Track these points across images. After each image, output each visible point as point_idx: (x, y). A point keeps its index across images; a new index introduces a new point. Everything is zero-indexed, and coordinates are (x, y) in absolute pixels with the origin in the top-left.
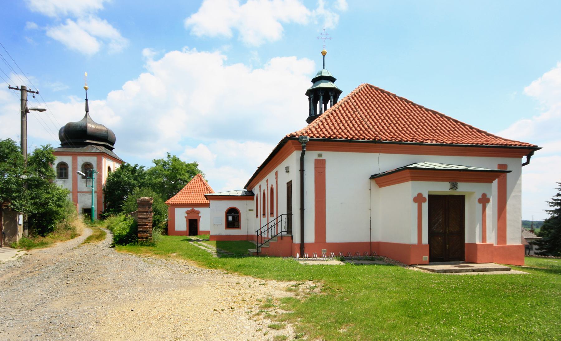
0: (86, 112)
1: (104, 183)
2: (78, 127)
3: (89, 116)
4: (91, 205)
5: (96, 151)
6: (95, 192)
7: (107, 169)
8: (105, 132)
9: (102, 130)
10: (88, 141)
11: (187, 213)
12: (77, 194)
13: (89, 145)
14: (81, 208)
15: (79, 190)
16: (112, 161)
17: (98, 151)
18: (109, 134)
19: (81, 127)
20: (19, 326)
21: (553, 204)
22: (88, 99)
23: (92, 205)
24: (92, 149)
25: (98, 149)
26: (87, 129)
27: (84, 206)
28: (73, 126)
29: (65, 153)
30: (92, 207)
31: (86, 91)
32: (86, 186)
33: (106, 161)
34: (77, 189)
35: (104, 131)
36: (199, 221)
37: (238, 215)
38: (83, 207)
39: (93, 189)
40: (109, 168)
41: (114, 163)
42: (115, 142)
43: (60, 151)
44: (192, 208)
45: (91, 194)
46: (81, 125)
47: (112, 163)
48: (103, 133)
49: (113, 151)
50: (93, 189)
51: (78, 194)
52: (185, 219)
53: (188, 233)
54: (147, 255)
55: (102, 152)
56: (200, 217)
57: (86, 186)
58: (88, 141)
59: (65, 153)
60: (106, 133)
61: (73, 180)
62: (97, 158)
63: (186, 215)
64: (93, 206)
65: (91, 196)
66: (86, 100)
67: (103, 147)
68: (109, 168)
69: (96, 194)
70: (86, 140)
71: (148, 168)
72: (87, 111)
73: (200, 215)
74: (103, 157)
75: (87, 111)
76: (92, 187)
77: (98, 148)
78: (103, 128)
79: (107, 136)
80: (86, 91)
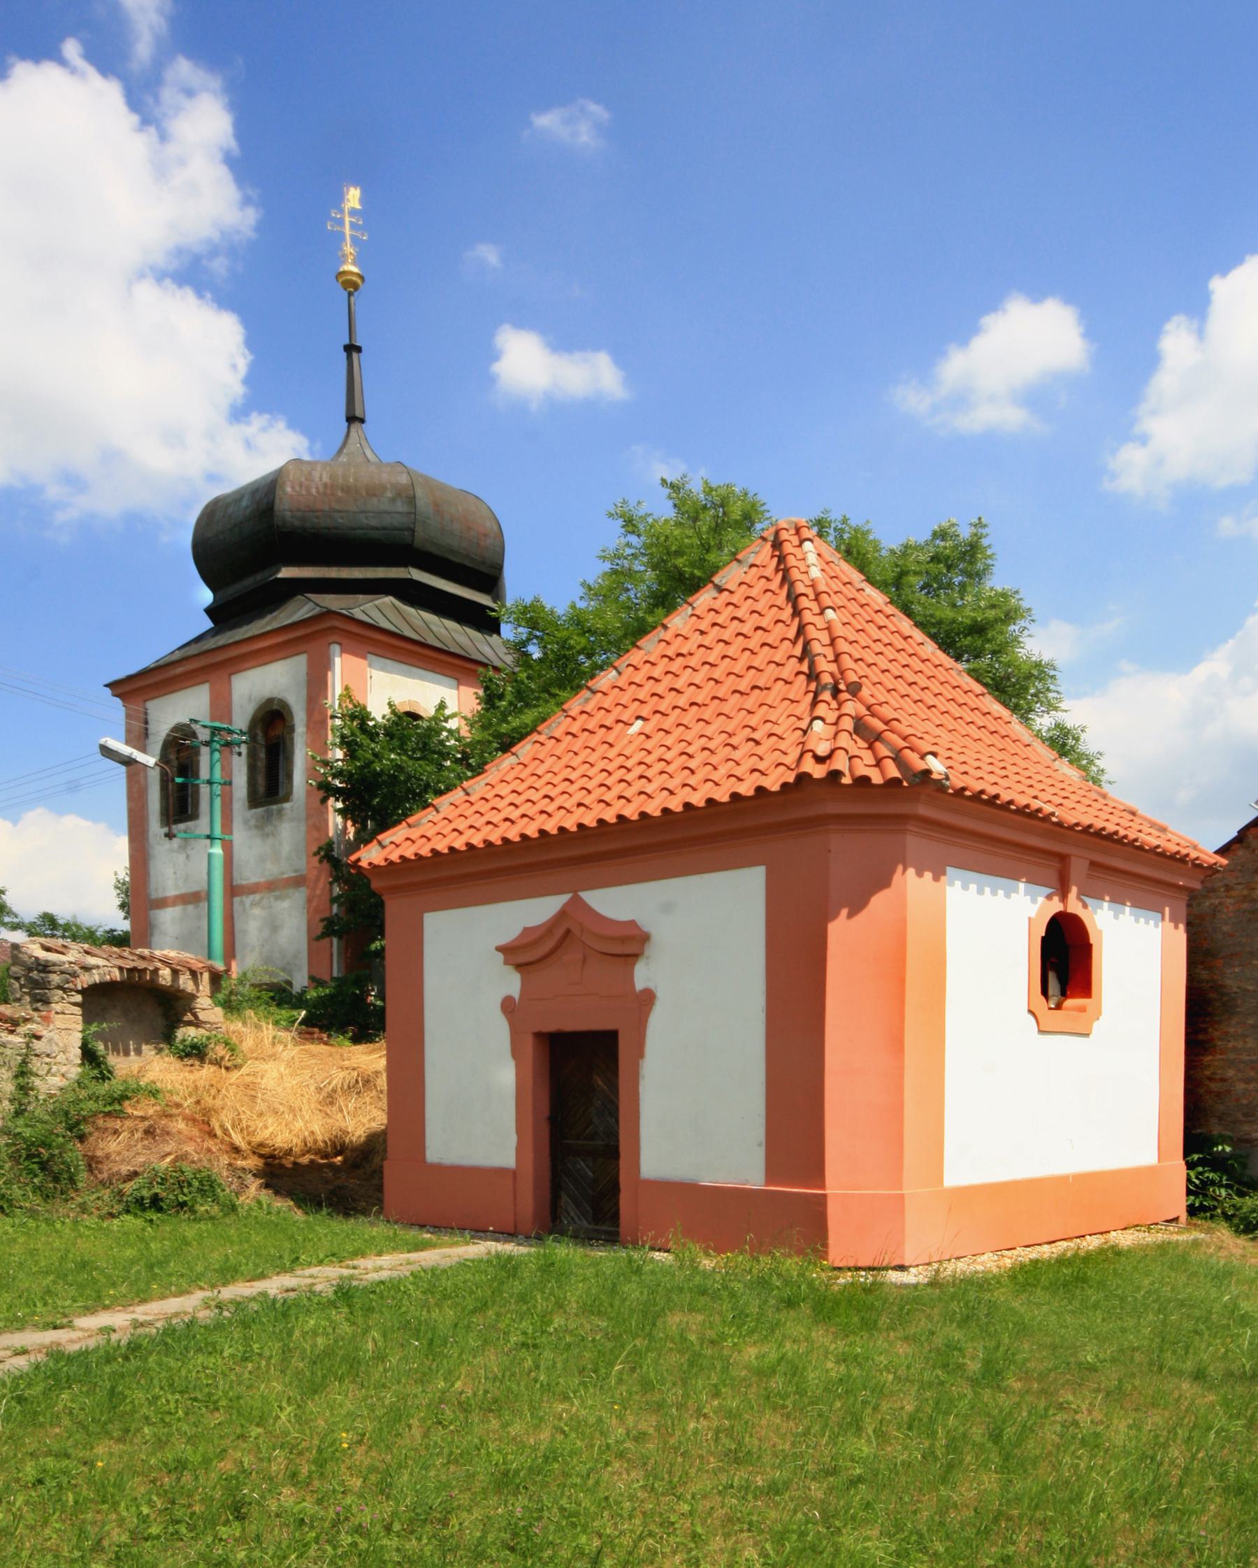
10: (286, 573)
11: (519, 967)
13: (299, 597)
16: (454, 682)
26: (277, 501)
36: (640, 1053)
37: (367, 972)
42: (499, 568)
44: (564, 899)
47: (455, 692)
52: (500, 1030)
53: (527, 1202)
54: (605, 1228)
56: (648, 998)
58: (286, 573)
59: (179, 670)
60: (400, 507)
63: (512, 984)
67: (389, 599)
70: (278, 571)
73: (643, 975)
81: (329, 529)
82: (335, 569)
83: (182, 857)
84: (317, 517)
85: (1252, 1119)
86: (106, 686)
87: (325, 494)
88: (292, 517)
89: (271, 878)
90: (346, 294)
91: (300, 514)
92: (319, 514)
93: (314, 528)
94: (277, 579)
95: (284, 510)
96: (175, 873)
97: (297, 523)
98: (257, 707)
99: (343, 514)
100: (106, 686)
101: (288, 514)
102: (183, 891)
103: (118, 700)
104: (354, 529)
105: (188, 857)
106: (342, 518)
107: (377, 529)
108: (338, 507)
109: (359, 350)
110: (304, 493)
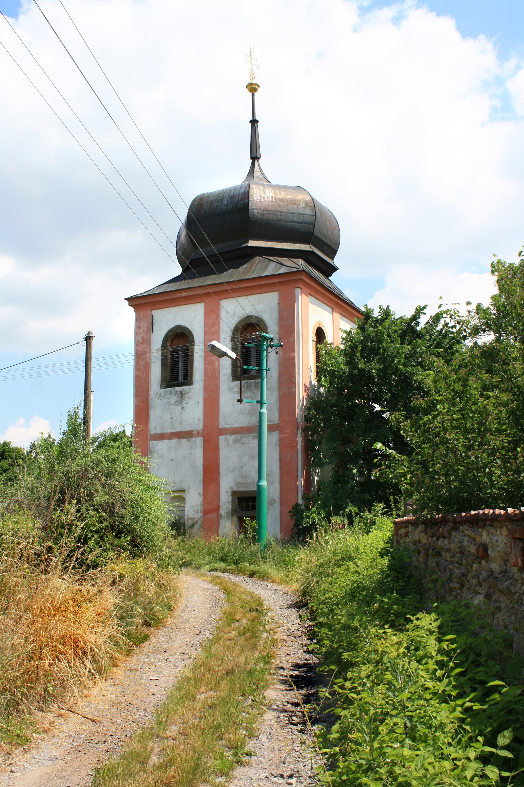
0: (251, 161)
1: (301, 397)
2: (225, 202)
3: (261, 171)
4: (256, 478)
5: (279, 269)
6: (271, 428)
7: (312, 336)
8: (305, 208)
9: (295, 202)
10: (252, 243)
12: (218, 440)
14: (230, 494)
15: (223, 424)
16: (331, 310)
17: (283, 270)
18: (318, 213)
19: (232, 197)
20: (486, 493)
21: (465, 580)
22: (257, 118)
23: (260, 478)
24: (265, 268)
25: (283, 264)
26: (251, 199)
27: (237, 484)
28: (212, 202)
29: (184, 294)
30: (259, 487)
31: (253, 95)
32: (240, 401)
33: (311, 305)
34: (218, 420)
35: (302, 205)
38: (235, 489)
39: (264, 410)
40: (320, 334)
41: (337, 315)
43: (173, 289)
45: (256, 434)
46: (232, 194)
48: (301, 209)
49: (334, 278)
50: (264, 410)
51: (222, 438)
55: (295, 270)
57: (240, 401)
58: (252, 243)
59: (184, 294)
60: (308, 211)
61: (206, 389)
62: (280, 297)
64: (264, 483)
65: (256, 442)
66: (251, 122)
67: (301, 260)
68: (320, 334)
69: (276, 435)
71: (468, 303)
72: (255, 157)
74: (298, 291)
75: (255, 157)
76: (261, 403)
77: (283, 262)
78: (301, 197)
79: (311, 219)
80: (253, 95)
81: (274, 221)
82: (275, 243)
83: (179, 408)
84: (269, 214)
85: (173, 495)
86: (126, 299)
87: (272, 201)
88: (257, 213)
89: (250, 425)
90: (251, 94)
91: (261, 212)
92: (270, 212)
93: (267, 220)
94: (248, 246)
95: (254, 209)
96: (171, 418)
97: (259, 216)
98: (239, 320)
99: (282, 214)
100: (126, 299)
101: (255, 211)
102: (178, 430)
103: (132, 309)
104: (286, 222)
105: (183, 408)
106: (281, 215)
107: (298, 223)
108: (279, 209)
109: (257, 122)
110: (263, 200)
